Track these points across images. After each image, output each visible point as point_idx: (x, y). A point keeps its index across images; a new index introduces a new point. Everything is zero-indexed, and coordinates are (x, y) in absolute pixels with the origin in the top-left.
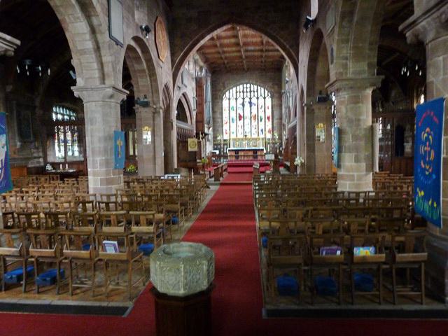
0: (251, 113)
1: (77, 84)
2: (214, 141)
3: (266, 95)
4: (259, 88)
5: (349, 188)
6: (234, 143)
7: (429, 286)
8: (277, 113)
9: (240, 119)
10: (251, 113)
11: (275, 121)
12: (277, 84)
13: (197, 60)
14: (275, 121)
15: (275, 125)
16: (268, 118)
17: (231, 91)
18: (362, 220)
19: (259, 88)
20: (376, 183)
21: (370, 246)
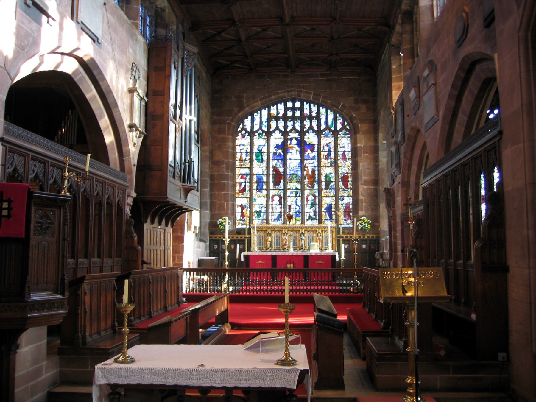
0: (261, 115)
1: (356, 397)
2: (211, 233)
3: (339, 126)
4: (323, 111)
5: (313, 99)
6: (260, 239)
7: (214, 325)
8: (364, 165)
9: (276, 183)
10: (261, 115)
11: (362, 188)
12: (365, 102)
13: (163, 10)
14: (362, 188)
15: (361, 197)
16: (345, 179)
17: (263, 111)
18: (347, 235)
19: (323, 111)
20: (461, 146)
21: (136, 193)
